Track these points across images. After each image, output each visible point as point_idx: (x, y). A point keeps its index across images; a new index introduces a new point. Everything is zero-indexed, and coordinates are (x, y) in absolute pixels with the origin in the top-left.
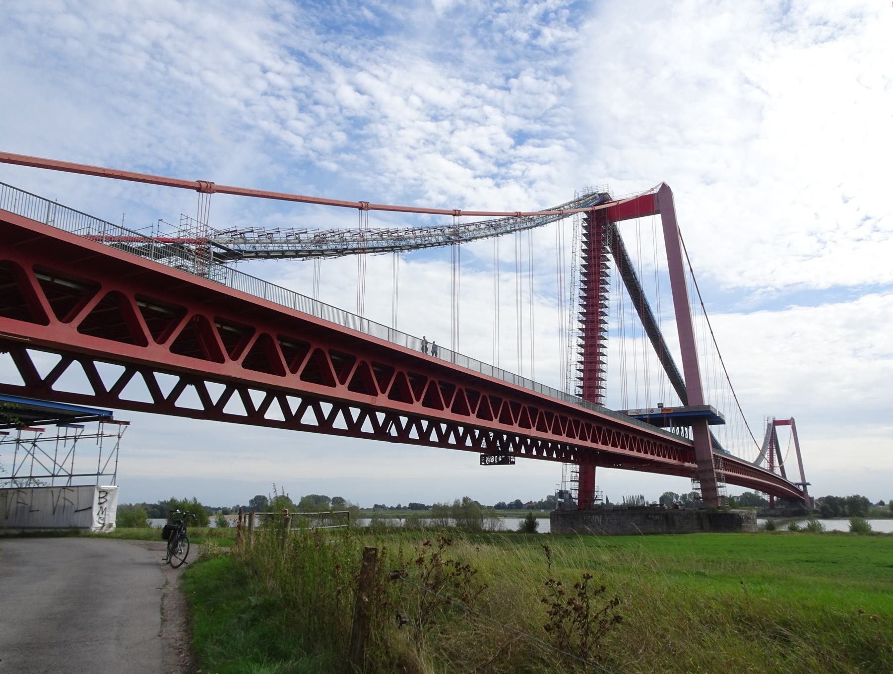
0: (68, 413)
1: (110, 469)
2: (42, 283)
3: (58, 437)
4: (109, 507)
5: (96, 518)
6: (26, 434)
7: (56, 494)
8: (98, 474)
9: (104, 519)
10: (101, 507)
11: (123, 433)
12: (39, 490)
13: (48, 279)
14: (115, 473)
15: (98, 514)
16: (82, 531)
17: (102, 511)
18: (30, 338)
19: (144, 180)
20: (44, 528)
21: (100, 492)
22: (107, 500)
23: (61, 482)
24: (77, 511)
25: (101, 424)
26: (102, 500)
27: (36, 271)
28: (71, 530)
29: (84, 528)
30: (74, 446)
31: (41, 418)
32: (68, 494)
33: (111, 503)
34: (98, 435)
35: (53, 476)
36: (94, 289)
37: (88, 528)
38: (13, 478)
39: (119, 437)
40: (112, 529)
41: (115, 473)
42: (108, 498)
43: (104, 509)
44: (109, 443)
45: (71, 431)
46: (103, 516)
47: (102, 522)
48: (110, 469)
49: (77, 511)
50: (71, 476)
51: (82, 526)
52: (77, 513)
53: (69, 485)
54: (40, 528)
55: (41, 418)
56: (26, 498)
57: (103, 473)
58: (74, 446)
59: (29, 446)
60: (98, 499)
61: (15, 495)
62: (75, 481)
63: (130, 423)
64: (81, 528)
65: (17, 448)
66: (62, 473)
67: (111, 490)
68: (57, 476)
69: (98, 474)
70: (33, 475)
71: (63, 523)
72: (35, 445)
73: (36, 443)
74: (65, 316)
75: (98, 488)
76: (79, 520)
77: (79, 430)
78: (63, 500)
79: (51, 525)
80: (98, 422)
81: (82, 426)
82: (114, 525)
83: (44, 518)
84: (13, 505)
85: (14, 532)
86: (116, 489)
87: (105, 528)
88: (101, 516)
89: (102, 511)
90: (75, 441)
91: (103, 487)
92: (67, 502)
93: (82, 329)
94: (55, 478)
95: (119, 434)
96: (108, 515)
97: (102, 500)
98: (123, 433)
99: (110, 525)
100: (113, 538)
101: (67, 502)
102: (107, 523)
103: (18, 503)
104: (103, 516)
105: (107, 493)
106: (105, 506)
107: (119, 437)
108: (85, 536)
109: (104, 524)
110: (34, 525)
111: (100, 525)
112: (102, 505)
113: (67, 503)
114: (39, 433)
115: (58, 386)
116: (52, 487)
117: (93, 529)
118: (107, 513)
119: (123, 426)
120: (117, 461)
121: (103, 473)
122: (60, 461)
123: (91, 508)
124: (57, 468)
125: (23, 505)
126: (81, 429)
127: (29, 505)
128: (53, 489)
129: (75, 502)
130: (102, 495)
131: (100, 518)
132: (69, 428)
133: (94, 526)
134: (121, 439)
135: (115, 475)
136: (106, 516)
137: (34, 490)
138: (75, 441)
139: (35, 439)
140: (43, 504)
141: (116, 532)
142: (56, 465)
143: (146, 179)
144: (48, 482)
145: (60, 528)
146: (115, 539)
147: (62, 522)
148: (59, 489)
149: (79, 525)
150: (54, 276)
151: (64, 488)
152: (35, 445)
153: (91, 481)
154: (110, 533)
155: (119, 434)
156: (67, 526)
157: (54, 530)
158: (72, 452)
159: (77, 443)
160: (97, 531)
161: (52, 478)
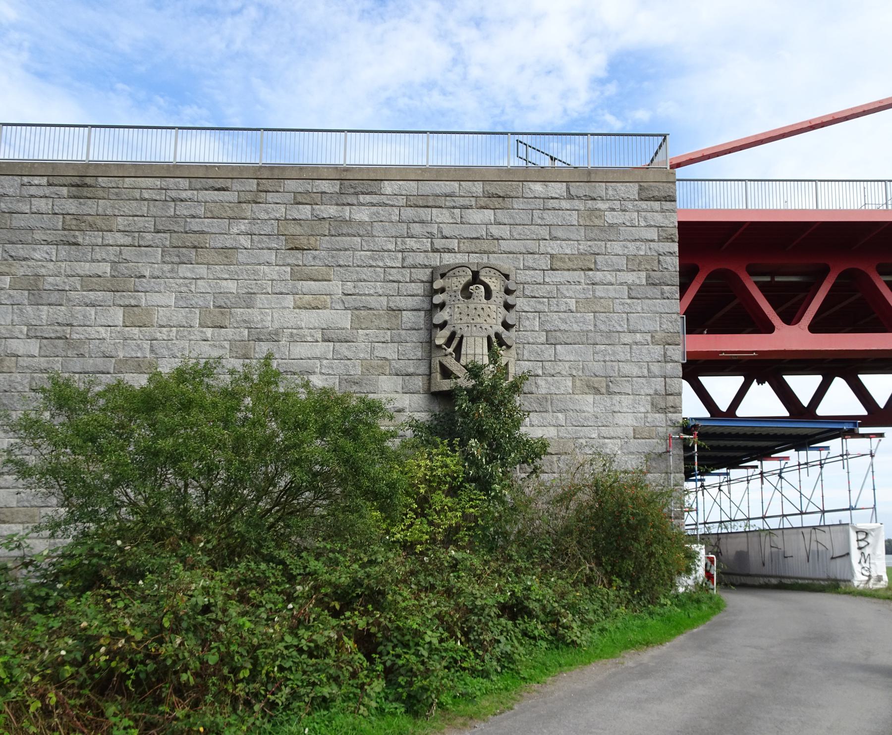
0: (805, 432)
1: (866, 500)
2: (762, 287)
3: (799, 465)
4: (874, 554)
5: (857, 568)
6: (769, 465)
7: (807, 537)
8: (851, 509)
9: (869, 570)
10: (862, 553)
11: (876, 450)
12: (733, 535)
13: (768, 279)
14: (875, 505)
15: (860, 562)
16: (842, 585)
17: (865, 558)
18: (756, 352)
19: (864, 111)
20: (789, 578)
21: (857, 532)
22: (868, 544)
23: (812, 520)
24: (832, 558)
25: (844, 440)
26: (862, 544)
27: (752, 274)
28: (830, 582)
29: (844, 581)
30: (821, 474)
31: (780, 443)
32: (820, 535)
33: (874, 549)
34: (842, 456)
35: (802, 513)
36: (820, 275)
37: (849, 581)
38: (764, 518)
39: (872, 456)
40: (882, 583)
41: (875, 505)
42: (870, 540)
43: (866, 555)
44: (859, 466)
45: (813, 455)
46: (867, 565)
47: (867, 574)
48: (866, 500)
49: (832, 558)
50: (823, 512)
51: (842, 578)
52: (833, 560)
53: (822, 524)
54: (797, 578)
55: (780, 443)
56: (777, 540)
57: (857, 507)
58: (821, 474)
59: (774, 479)
60: (856, 543)
61: (768, 538)
62: (830, 519)
63: (885, 435)
64: (840, 580)
65: (762, 483)
66: (811, 508)
67: (873, 530)
68: (806, 513)
69: (851, 509)
70: (785, 513)
71: (820, 573)
72: (781, 477)
73: (783, 475)
74: (790, 318)
75: (854, 528)
76: (836, 570)
77: (824, 453)
78: (816, 543)
79: (807, 575)
80: (840, 439)
81: (827, 448)
82: (885, 578)
83: (799, 568)
84: (768, 551)
85: (774, 581)
86: (879, 528)
87: (872, 581)
88: (864, 565)
89: (865, 558)
90: (821, 468)
91: (861, 525)
92: (820, 547)
93: (815, 327)
94: (804, 516)
95: (871, 451)
96: (874, 564)
97: (862, 544)
98: (876, 450)
99: (879, 579)
100: (879, 597)
101: (820, 547)
102: (874, 574)
103: (771, 547)
104: (867, 565)
105: (867, 534)
106: (867, 551)
107: (872, 456)
108: (845, 593)
109: (870, 576)
110: (791, 574)
111: (867, 578)
112: (863, 550)
113: (821, 548)
114: (783, 462)
115: (822, 410)
116: (803, 527)
117: (856, 583)
118: (872, 561)
119: (875, 440)
120: (874, 489)
121: (857, 507)
122: (807, 492)
123: (848, 554)
124: (804, 500)
125: (776, 549)
126: (826, 452)
127: (783, 550)
128: (803, 530)
129: (828, 546)
130: (861, 536)
131: (863, 568)
132: (809, 452)
133: (856, 579)
134: (874, 458)
135: (874, 508)
136: (872, 566)
137: (785, 531)
138: (821, 468)
139: (781, 469)
140: (796, 548)
141: (888, 588)
142: (803, 498)
143: (866, 109)
144: (796, 522)
145: (818, 580)
146: (881, 601)
147: (818, 572)
148: (809, 530)
149: (838, 577)
150: (772, 274)
151: (814, 528)
152: (781, 477)
153: (844, 517)
154: (877, 590)
155: (871, 451)
156: (825, 577)
157: (810, 582)
158: (820, 482)
159: (823, 469)
160: (862, 585)
161: (800, 516)
